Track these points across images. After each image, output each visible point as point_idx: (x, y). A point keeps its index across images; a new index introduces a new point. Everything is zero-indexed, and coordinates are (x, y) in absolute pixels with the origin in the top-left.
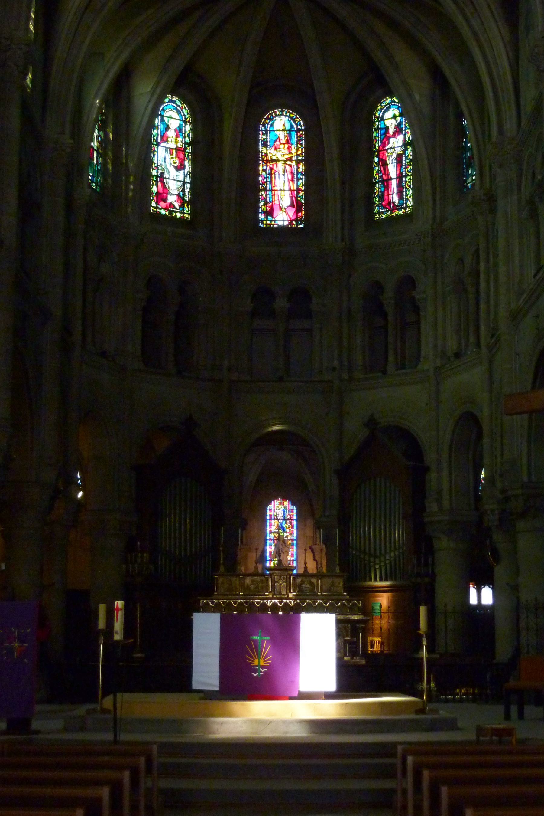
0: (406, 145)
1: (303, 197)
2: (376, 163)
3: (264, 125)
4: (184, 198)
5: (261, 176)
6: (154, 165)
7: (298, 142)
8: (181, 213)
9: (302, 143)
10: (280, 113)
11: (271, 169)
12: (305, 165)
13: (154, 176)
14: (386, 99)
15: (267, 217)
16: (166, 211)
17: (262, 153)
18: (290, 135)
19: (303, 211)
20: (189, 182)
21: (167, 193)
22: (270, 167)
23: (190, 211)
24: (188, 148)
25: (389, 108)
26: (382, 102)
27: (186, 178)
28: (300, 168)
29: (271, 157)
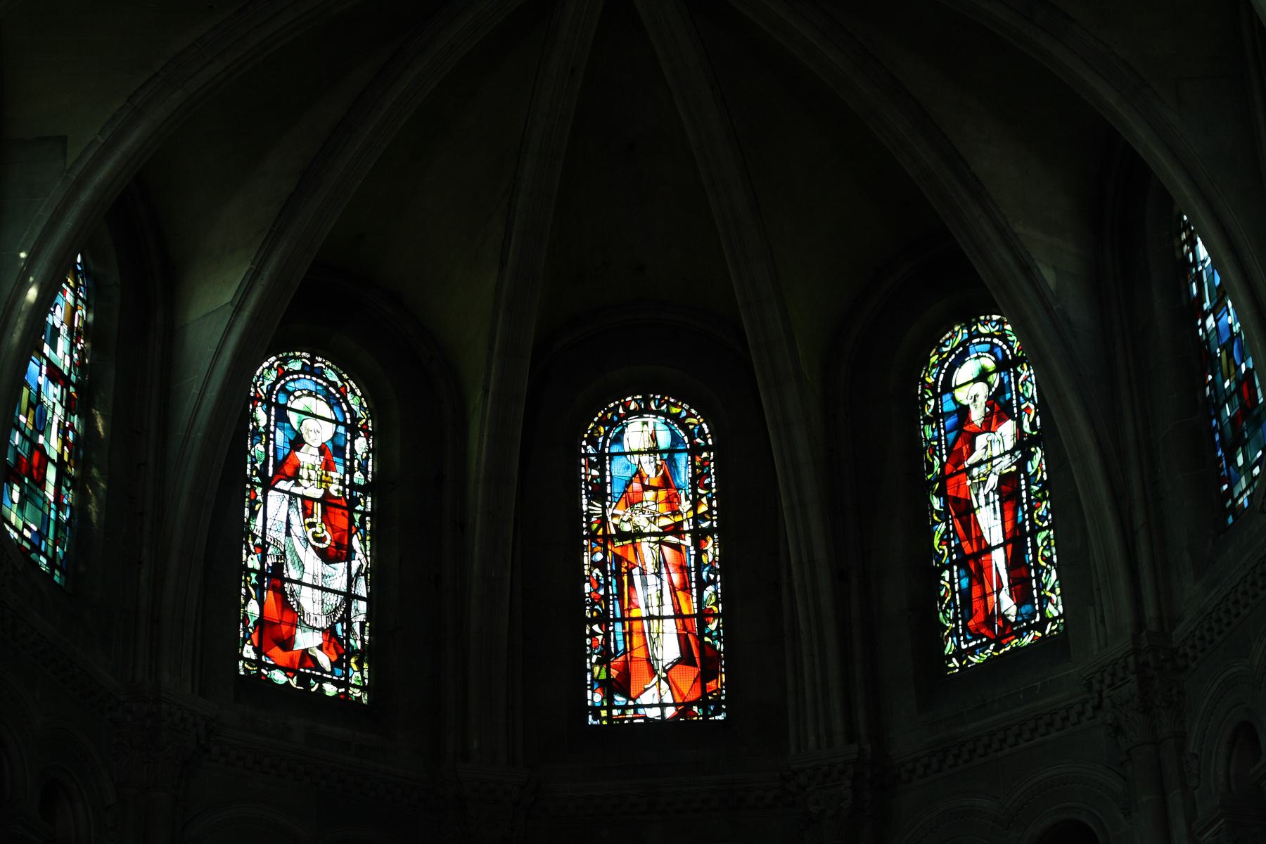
0: (1023, 445)
1: (719, 633)
2: (938, 513)
3: (592, 441)
4: (348, 643)
5: (589, 581)
6: (254, 540)
7: (696, 480)
8: (337, 684)
9: (711, 482)
10: (640, 406)
11: (619, 559)
12: (722, 544)
13: (253, 570)
14: (954, 333)
15: (611, 700)
16: (288, 677)
17: (589, 516)
18: (671, 462)
19: (722, 673)
20: (365, 595)
21: (294, 625)
22: (615, 554)
23: (366, 681)
24: (362, 500)
25: (966, 353)
26: (941, 341)
27: (353, 584)
28: (706, 552)
29: (616, 526)
